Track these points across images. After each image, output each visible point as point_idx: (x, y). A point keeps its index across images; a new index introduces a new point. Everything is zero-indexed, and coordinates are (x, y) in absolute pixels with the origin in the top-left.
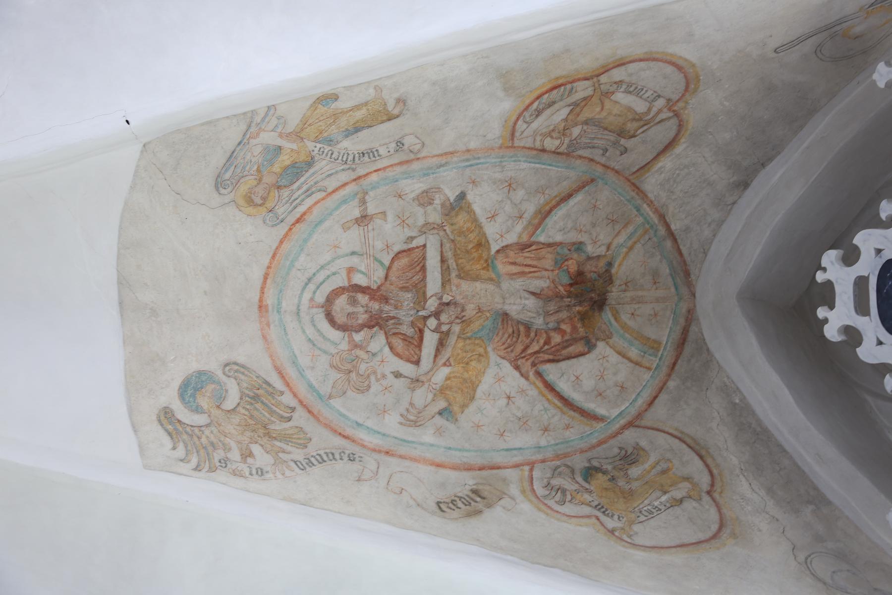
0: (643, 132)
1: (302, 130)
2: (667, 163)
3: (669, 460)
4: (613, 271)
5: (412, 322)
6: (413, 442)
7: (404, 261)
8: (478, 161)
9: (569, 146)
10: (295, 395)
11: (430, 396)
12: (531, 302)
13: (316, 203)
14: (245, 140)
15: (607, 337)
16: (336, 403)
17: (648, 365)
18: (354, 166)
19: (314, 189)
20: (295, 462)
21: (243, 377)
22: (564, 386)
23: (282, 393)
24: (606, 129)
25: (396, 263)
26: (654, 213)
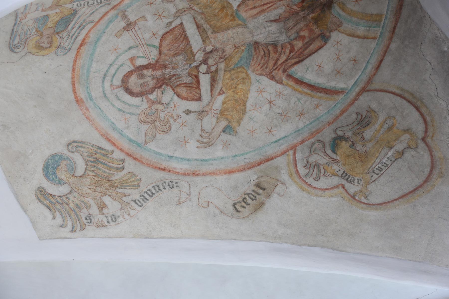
3: (394, 117)
5: (189, 73)
6: (210, 159)
7: (170, 38)
10: (122, 150)
11: (214, 120)
12: (274, 27)
13: (90, 31)
15: (338, 27)
16: (151, 146)
17: (373, 35)
19: (84, 24)
20: (135, 201)
21: (82, 149)
22: (311, 78)
23: (112, 152)
25: (164, 42)
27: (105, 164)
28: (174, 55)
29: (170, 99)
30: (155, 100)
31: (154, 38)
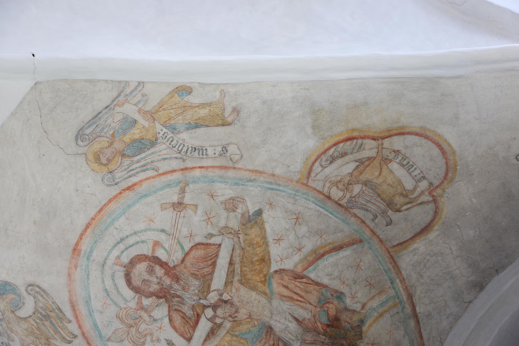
0: (407, 209)
1: (157, 112)
2: (420, 245)
4: (364, 329)
5: (193, 306)
7: (200, 252)
8: (278, 188)
9: (349, 202)
10: (80, 327)
12: (293, 326)
14: (112, 106)
18: (185, 157)
19: (149, 167)
21: (41, 299)
23: (70, 322)
24: (379, 195)
26: (404, 291)
27: (54, 325)
28: (193, 274)
29: (160, 317)
30: (146, 307)
31: (188, 239)
